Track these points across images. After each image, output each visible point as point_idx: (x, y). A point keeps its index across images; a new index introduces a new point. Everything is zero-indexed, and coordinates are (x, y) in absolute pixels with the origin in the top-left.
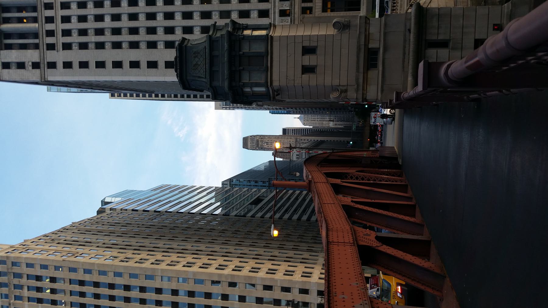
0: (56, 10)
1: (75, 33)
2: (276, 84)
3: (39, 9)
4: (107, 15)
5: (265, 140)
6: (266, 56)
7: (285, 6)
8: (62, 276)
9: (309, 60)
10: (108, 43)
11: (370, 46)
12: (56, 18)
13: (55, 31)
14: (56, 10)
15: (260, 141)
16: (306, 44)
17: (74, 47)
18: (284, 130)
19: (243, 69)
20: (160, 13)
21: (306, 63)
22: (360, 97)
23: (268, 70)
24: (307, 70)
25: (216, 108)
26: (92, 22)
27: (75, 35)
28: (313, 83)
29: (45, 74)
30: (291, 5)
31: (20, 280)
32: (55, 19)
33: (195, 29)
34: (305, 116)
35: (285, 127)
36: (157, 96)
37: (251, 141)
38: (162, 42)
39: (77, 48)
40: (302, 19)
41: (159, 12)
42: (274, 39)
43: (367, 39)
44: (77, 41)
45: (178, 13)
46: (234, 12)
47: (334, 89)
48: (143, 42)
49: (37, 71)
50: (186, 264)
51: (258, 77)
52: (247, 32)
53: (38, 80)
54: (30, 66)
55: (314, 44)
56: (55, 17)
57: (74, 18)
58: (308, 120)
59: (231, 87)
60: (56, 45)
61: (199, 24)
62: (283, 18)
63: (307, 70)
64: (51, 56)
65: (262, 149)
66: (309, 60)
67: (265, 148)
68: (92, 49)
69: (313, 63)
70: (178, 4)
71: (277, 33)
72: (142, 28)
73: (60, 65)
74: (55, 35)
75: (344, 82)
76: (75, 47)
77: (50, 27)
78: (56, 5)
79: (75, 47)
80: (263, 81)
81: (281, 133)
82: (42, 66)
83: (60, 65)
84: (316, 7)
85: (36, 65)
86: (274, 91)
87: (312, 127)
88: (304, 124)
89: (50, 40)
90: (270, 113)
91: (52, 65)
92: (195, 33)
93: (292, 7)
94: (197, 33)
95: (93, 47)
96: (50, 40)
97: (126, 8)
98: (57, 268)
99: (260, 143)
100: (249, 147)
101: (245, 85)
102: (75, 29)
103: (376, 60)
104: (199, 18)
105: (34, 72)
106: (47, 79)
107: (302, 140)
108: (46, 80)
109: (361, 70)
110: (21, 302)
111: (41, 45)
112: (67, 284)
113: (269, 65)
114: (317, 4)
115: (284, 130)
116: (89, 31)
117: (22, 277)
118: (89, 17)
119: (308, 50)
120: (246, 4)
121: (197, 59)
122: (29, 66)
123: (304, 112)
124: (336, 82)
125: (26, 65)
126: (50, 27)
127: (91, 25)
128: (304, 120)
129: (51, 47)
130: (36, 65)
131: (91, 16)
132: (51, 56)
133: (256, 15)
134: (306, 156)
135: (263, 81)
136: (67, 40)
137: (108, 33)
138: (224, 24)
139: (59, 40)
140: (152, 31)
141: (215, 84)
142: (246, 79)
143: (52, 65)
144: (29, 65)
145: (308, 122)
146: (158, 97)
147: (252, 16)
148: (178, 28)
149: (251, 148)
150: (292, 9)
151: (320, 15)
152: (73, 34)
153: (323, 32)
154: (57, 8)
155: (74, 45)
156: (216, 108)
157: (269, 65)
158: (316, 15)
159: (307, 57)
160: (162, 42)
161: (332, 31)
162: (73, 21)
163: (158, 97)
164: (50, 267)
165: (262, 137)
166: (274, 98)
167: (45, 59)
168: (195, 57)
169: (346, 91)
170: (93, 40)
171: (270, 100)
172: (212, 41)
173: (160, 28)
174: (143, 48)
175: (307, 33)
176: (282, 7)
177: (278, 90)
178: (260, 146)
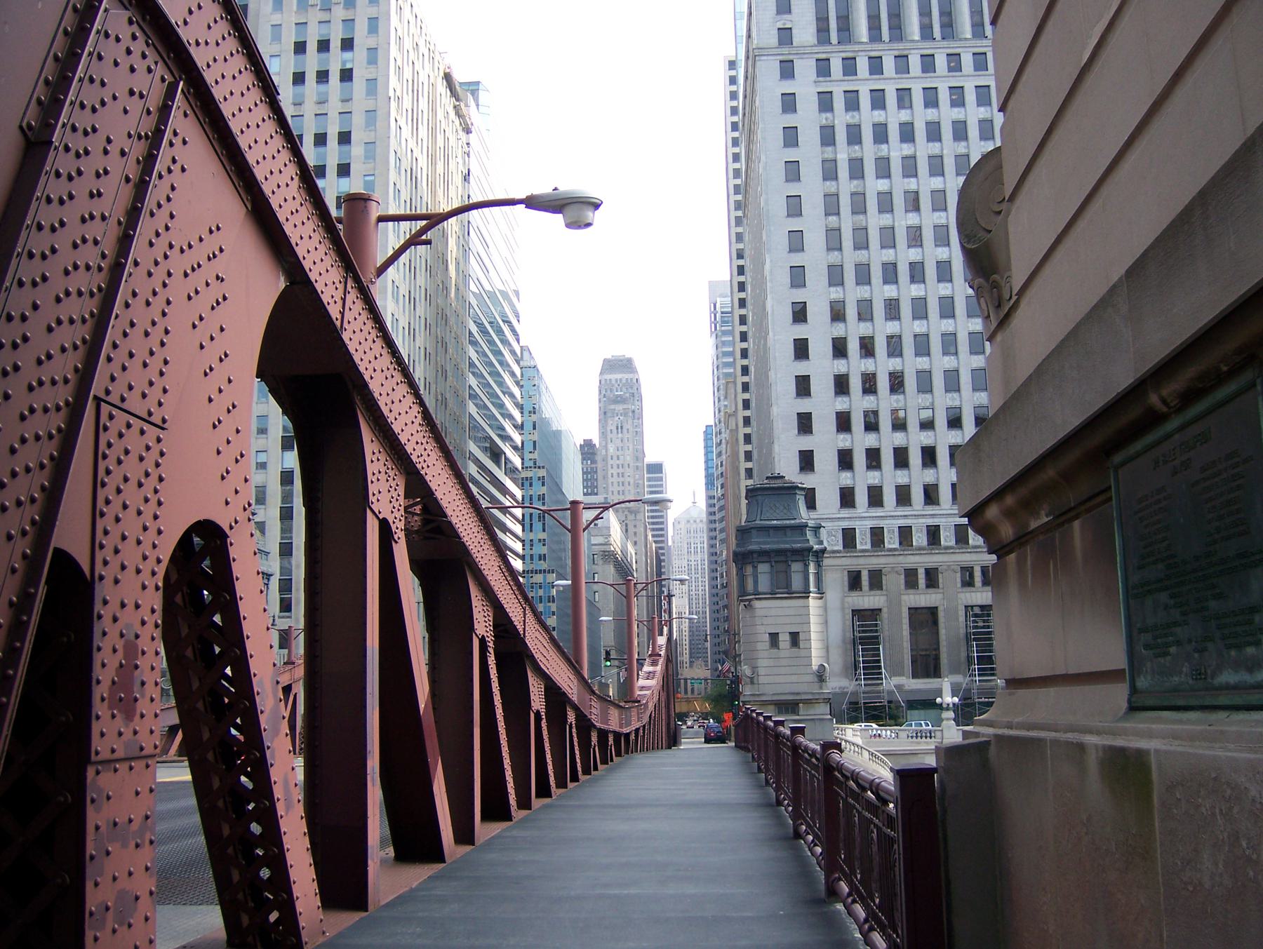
0: (895, 79)
1: (853, 117)
2: (757, 604)
3: (896, 45)
4: (889, 184)
5: (630, 421)
6: (790, 594)
7: (919, 537)
8: (356, 96)
9: (784, 639)
10: (836, 187)
11: (801, 705)
12: (880, 79)
13: (854, 77)
14: (895, 79)
15: (625, 406)
16: (802, 636)
17: (824, 115)
18: (656, 468)
19: (772, 566)
20: (896, 291)
21: (781, 637)
22: (747, 699)
23: (772, 595)
24: (774, 638)
25: (713, 285)
26: (876, 153)
27: (848, 117)
28: (760, 646)
29: (768, 55)
30: (920, 549)
31: (342, 5)
32: (877, 77)
33: (870, 360)
34: (701, 521)
35: (666, 468)
36: (739, 221)
37: (624, 381)
38: (842, 296)
39: (824, 122)
40: (896, 569)
41: (898, 289)
42: (806, 600)
43: (808, 702)
44: (836, 122)
45: (898, 327)
46: (905, 438)
47: (754, 669)
48: (840, 257)
49: (773, 40)
50: (608, 573)
51: (764, 584)
52: (812, 569)
53: (755, 42)
54: (784, 24)
55: (802, 645)
56: (881, 76)
57: (880, 115)
58: (689, 532)
59: (752, 552)
60: (828, 79)
61: (879, 369)
62: (897, 534)
63: (774, 638)
64: (805, 69)
65: (604, 415)
66: (784, 639)
67: (606, 421)
68: (823, 153)
69: (782, 645)
70: (915, 327)
71: (813, 602)
72: (867, 256)
73: (788, 87)
74: (846, 78)
75: (762, 680)
76: (825, 118)
77: (863, 65)
78: (904, 80)
79: (825, 118)
80: (760, 589)
81: (650, 458)
82: (785, 50)
83: (788, 87)
84: (917, 597)
85: (785, 35)
86: (750, 600)
87: (670, 543)
88: (677, 522)
89: (836, 66)
90: (707, 426)
91: (787, 70)
92: (863, 361)
93: (916, 550)
94: (863, 365)
95: (826, 156)
96: (836, 66)
97: (903, 223)
98: (372, 82)
99: (620, 407)
100: (608, 377)
101: (755, 567)
102: (860, 119)
103: (787, 712)
104: (891, 369)
105: (772, 32)
106: (760, 60)
107: (635, 526)
108: (757, 58)
109: (775, 698)
110: (295, 8)
111: (828, 48)
112: (340, 107)
113: (778, 596)
114: (922, 597)
115: (656, 468)
116: (857, 147)
117: (347, 9)
118: (884, 147)
119: (795, 638)
120: (919, 461)
121: (782, 508)
122: (782, 22)
123: (713, 518)
124: (761, 671)
125: (786, 16)
126: (863, 65)
127: (869, 151)
128: (688, 521)
129: (823, 68)
130: (785, 35)
131: (886, 150)
132: (805, 69)
133: (900, 481)
134: (597, 547)
135: (760, 589)
136: (839, 102)
137: (855, 185)
138: (822, 539)
139: (838, 86)
140: (907, 133)
141: (754, 532)
142: (763, 568)
143: (787, 70)
144: (784, 21)
145: (684, 532)
146: (736, 209)
147: (899, 472)
148: (871, 328)
149: (603, 382)
150: (913, 550)
151: (903, 603)
152: (850, 114)
153: (814, 653)
154: (900, 80)
155: (829, 115)
156: (713, 285)
157: (778, 596)
158: (904, 598)
159: (787, 637)
160: (842, 296)
161: (815, 664)
162: (876, 113)
163: (736, 209)
164: (372, 69)
165: (637, 415)
166: (742, 601)
167: (798, 56)
168: (784, 506)
169: (752, 683)
170: (839, 156)
171: (739, 596)
172: (802, 528)
173: (869, 291)
174: (829, 257)
175: (813, 636)
176: (917, 532)
177: (750, 606)
178: (613, 407)
